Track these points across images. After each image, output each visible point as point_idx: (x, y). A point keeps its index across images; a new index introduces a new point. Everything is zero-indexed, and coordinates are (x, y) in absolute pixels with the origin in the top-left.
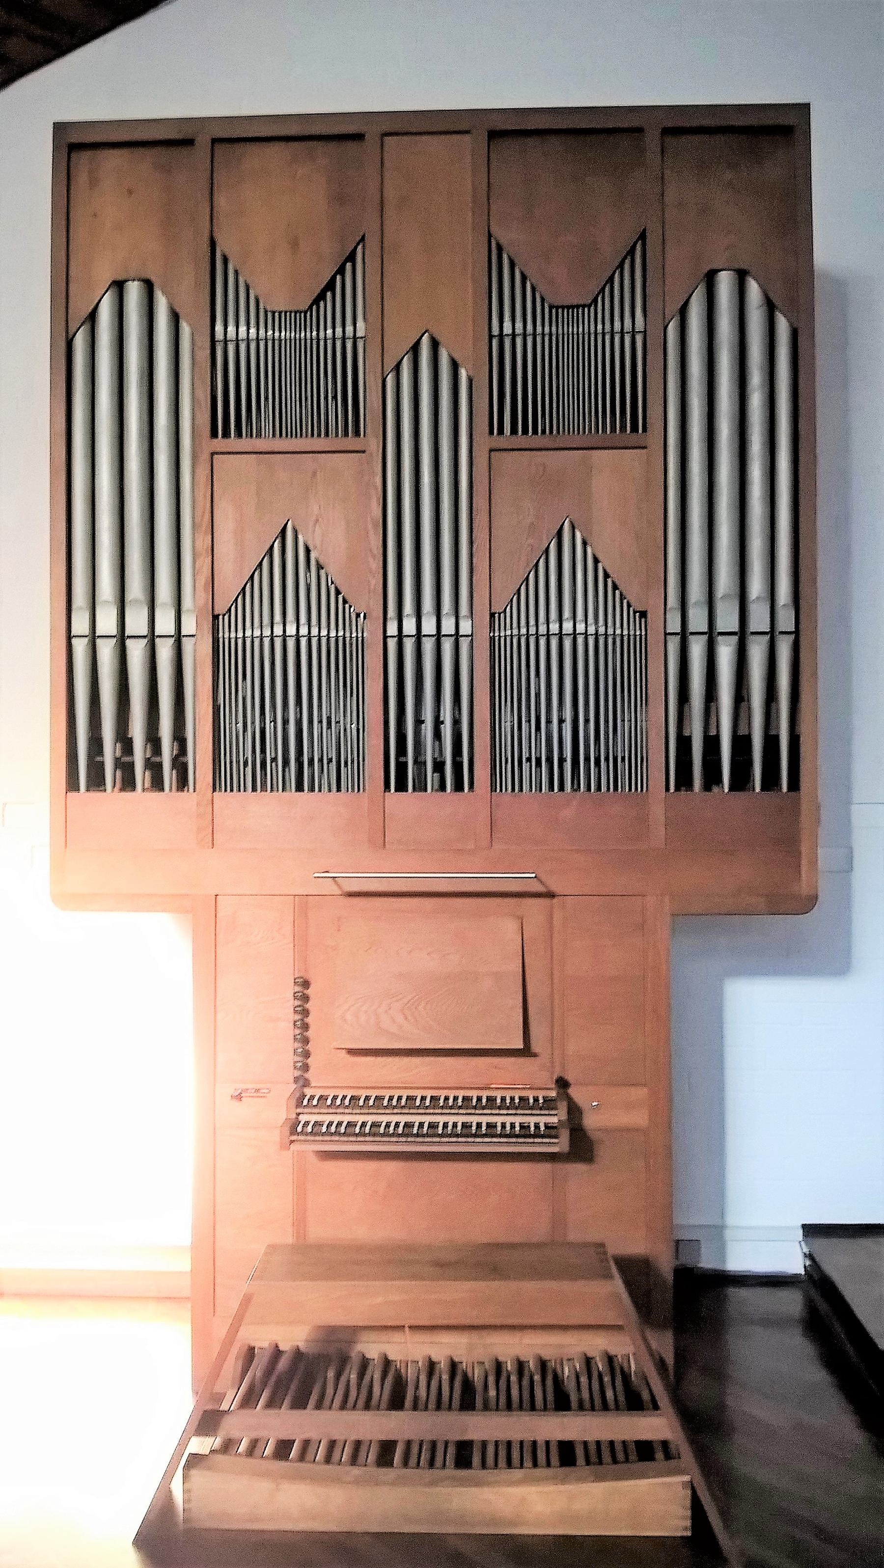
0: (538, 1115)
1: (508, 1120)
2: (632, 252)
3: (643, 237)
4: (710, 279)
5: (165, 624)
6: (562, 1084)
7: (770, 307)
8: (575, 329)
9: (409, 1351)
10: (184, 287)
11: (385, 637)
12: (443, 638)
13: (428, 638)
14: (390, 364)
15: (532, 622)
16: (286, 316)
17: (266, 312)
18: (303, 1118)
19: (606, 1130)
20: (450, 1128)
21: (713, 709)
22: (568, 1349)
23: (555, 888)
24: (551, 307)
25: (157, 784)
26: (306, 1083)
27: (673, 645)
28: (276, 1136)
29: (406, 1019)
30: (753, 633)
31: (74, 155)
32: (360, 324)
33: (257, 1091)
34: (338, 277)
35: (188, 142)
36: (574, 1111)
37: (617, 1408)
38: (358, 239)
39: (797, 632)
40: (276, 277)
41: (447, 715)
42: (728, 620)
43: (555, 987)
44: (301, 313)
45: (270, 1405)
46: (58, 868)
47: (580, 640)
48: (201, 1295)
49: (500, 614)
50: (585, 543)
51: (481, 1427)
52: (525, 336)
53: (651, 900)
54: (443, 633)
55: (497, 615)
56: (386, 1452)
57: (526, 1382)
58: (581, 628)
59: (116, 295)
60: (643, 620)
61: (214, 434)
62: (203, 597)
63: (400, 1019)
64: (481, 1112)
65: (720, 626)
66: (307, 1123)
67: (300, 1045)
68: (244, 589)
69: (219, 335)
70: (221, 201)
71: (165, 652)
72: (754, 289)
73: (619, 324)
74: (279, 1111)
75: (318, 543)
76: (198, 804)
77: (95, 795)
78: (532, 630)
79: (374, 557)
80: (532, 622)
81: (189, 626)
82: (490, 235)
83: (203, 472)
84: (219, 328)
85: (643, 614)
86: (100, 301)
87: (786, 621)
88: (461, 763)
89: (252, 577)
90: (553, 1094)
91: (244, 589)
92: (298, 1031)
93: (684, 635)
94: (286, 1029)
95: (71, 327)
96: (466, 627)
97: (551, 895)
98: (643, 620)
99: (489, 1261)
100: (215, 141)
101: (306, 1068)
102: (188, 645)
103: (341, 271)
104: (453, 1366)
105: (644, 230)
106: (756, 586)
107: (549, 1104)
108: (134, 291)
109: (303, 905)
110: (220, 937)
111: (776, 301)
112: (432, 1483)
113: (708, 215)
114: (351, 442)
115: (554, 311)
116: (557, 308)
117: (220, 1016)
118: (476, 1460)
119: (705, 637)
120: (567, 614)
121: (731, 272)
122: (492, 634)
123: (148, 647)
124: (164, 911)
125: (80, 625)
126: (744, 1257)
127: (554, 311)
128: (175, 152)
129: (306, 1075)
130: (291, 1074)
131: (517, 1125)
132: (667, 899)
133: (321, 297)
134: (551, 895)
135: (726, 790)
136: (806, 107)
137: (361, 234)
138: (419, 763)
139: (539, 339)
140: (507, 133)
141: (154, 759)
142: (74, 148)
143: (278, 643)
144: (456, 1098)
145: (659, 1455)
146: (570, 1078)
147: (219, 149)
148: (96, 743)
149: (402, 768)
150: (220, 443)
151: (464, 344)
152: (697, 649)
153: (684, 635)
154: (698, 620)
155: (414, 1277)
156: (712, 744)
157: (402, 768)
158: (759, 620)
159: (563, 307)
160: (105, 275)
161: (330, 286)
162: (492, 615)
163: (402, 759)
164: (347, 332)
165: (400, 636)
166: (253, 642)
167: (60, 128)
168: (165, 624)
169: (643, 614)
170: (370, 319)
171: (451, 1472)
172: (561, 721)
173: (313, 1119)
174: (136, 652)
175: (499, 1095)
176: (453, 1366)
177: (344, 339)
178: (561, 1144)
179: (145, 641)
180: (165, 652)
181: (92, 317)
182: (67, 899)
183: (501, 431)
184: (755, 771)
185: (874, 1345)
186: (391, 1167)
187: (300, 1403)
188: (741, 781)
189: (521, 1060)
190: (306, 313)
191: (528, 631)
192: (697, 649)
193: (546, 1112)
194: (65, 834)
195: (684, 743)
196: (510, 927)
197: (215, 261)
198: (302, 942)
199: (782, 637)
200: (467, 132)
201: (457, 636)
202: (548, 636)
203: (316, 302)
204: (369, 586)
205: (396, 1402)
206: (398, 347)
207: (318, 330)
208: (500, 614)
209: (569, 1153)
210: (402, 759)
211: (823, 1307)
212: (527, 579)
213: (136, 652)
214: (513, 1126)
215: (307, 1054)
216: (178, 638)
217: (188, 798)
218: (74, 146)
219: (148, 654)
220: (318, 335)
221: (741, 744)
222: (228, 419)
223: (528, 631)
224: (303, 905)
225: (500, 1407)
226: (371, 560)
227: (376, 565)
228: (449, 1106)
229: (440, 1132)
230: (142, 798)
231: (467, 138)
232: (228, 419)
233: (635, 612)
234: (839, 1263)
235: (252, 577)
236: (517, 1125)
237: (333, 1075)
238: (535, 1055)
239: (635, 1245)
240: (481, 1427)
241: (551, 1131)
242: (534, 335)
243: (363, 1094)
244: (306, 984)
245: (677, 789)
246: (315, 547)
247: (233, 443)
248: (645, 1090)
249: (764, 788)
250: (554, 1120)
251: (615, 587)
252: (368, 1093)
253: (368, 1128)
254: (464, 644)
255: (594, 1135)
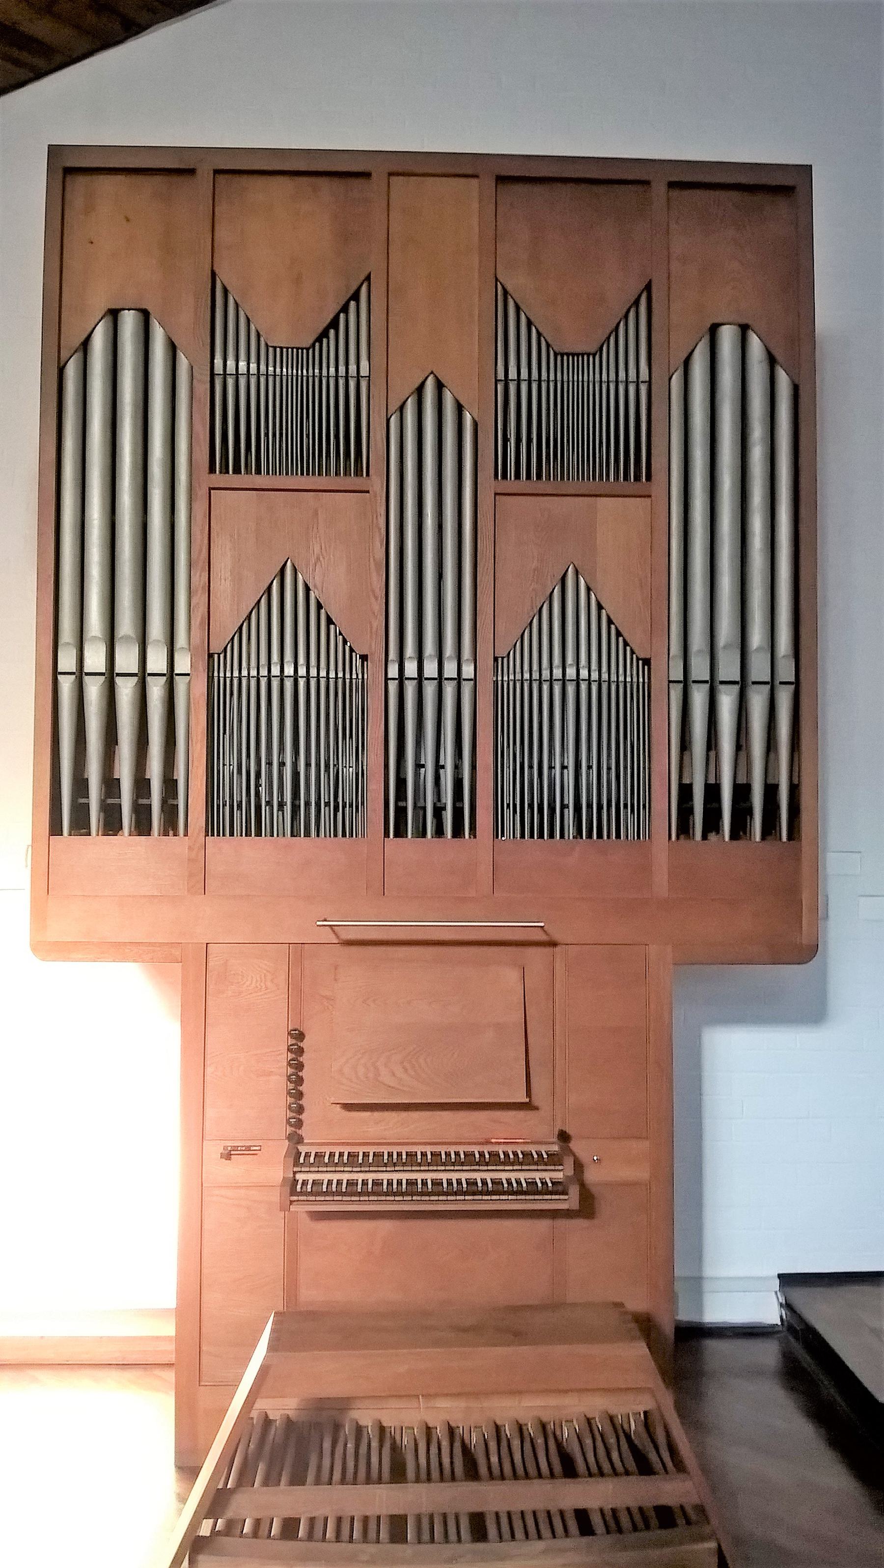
0: (375, 1171)
1: (395, 1177)
2: (637, 303)
3: (648, 288)
4: (714, 330)
5: (157, 662)
6: (564, 1137)
7: (772, 361)
8: (317, 371)
9: (406, 1417)
10: (187, 316)
11: (387, 679)
12: (406, 682)
13: (410, 682)
14: (394, 405)
15: (535, 667)
16: (287, 351)
17: (267, 346)
18: (300, 1177)
19: (607, 1184)
20: (334, 1186)
21: (796, 759)
22: (569, 1410)
23: (557, 936)
24: (556, 355)
25: (143, 827)
26: (300, 1140)
27: (676, 693)
28: (275, 1196)
29: (406, 1070)
30: (754, 683)
31: (68, 178)
32: (364, 363)
33: (248, 1148)
34: (342, 315)
35: (191, 172)
36: (579, 1166)
37: (552, 1475)
38: (362, 277)
39: (797, 683)
40: (280, 314)
41: (448, 759)
42: (729, 669)
43: (557, 1038)
44: (302, 349)
45: (266, 1483)
46: (39, 914)
47: (584, 686)
48: (191, 1365)
49: (219, 654)
50: (589, 589)
51: (494, 1497)
52: (519, 380)
53: (653, 949)
54: (176, 672)
55: (216, 656)
56: (398, 1528)
57: (434, 1450)
58: (584, 673)
59: (111, 325)
60: (646, 667)
61: (212, 470)
62: (198, 635)
63: (400, 1072)
64: (485, 1168)
65: (722, 675)
66: (305, 1183)
67: (293, 1100)
68: (241, 628)
69: (219, 369)
70: (222, 233)
71: (156, 691)
72: (755, 344)
73: (344, 368)
74: (275, 1171)
75: (319, 585)
76: (190, 848)
77: (79, 841)
78: (536, 676)
79: (376, 598)
80: (535, 667)
81: (183, 664)
82: (213, 275)
83: (200, 508)
84: (218, 361)
85: (647, 662)
86: (94, 329)
87: (786, 671)
88: (462, 809)
89: (249, 617)
90: (555, 1148)
91: (241, 628)
92: (291, 1086)
93: (686, 683)
94: (278, 1082)
95: (62, 356)
96: (468, 671)
97: (553, 944)
98: (646, 667)
99: (509, 1324)
100: (217, 172)
101: (299, 1124)
102: (181, 685)
103: (345, 309)
104: (451, 1431)
105: (650, 280)
106: (757, 637)
107: (554, 1160)
108: (129, 322)
109: (298, 953)
110: (211, 988)
111: (778, 355)
112: (451, 1560)
113: (710, 272)
114: (352, 482)
115: (559, 358)
116: (562, 355)
117: (209, 1070)
118: (492, 1531)
119: (707, 686)
120: (570, 659)
121: (732, 326)
122: (495, 679)
123: (107, 684)
124: (135, 961)
125: (67, 662)
126: (720, 1310)
127: (559, 358)
128: (175, 179)
129: (299, 1132)
130: (282, 1130)
131: (404, 1182)
132: (669, 949)
133: (325, 334)
134: (553, 944)
135: (727, 838)
136: (807, 170)
137: (367, 273)
138: (420, 809)
139: (544, 385)
140: (515, 177)
141: (110, 801)
142: (69, 171)
143: (275, 683)
144: (341, 1155)
145: (681, 1521)
146: (570, 1130)
147: (221, 178)
148: (81, 785)
149: (401, 812)
150: (218, 479)
151: (470, 386)
152: (699, 698)
153: (686, 683)
154: (700, 669)
155: (437, 1343)
156: (713, 792)
157: (401, 812)
158: (759, 669)
159: (568, 355)
160: (100, 303)
161: (334, 324)
162: (496, 659)
163: (401, 804)
164: (350, 371)
165: (80, 674)
166: (508, 684)
167: (54, 151)
168: (157, 662)
169: (647, 662)
170: (374, 359)
171: (468, 1546)
172: (282, 764)
173: (311, 1177)
174: (126, 690)
175: (500, 1150)
176: (451, 1431)
177: (337, 377)
178: (571, 1201)
179: (135, 679)
180: (156, 691)
181: (85, 345)
182: (49, 948)
183: (505, 476)
184: (767, 818)
185: (876, 1401)
186: (386, 1226)
187: (298, 1479)
188: (740, 828)
189: (521, 1114)
190: (308, 349)
191: (540, 675)
192: (699, 698)
193: (552, 1168)
194: (46, 882)
195: (686, 791)
196: (512, 976)
197: (216, 292)
198: (297, 994)
199: (722, 688)
200: (475, 176)
201: (459, 680)
202: (551, 681)
203: (319, 340)
204: (371, 628)
205: (398, 1474)
206: (403, 387)
207: (321, 369)
208: (219, 654)
209: (580, 1211)
210: (401, 804)
211: (806, 1359)
212: (531, 624)
213: (126, 690)
214: (400, 1182)
215: (300, 1109)
216: (171, 675)
217: (177, 844)
218: (70, 170)
219: (76, 694)
220: (321, 373)
221: (742, 792)
222: (231, 453)
223: (540, 675)
224: (298, 953)
225: (383, 1479)
226: (373, 599)
227: (378, 607)
228: (394, 1162)
229: (359, 1190)
230: (126, 842)
231: (474, 182)
232: (231, 453)
233: (638, 659)
234: (824, 1314)
235: (249, 617)
236: (404, 1182)
237: (326, 1129)
238: (536, 1108)
239: (638, 1303)
240: (494, 1497)
241: (559, 1188)
242: (540, 381)
243: (327, 1150)
244: (301, 1036)
245: (678, 837)
246: (315, 586)
247: (231, 479)
248: (647, 1144)
249: (764, 837)
250: (559, 1176)
251: (619, 634)
252: (399, 1149)
253: (309, 1187)
254: (467, 688)
255: (594, 1190)
